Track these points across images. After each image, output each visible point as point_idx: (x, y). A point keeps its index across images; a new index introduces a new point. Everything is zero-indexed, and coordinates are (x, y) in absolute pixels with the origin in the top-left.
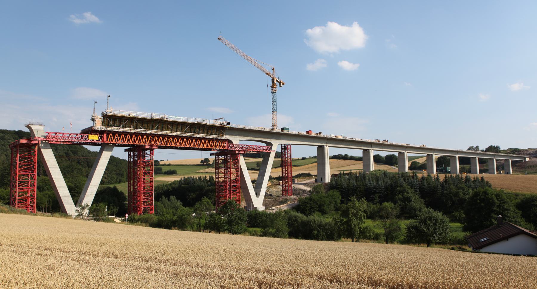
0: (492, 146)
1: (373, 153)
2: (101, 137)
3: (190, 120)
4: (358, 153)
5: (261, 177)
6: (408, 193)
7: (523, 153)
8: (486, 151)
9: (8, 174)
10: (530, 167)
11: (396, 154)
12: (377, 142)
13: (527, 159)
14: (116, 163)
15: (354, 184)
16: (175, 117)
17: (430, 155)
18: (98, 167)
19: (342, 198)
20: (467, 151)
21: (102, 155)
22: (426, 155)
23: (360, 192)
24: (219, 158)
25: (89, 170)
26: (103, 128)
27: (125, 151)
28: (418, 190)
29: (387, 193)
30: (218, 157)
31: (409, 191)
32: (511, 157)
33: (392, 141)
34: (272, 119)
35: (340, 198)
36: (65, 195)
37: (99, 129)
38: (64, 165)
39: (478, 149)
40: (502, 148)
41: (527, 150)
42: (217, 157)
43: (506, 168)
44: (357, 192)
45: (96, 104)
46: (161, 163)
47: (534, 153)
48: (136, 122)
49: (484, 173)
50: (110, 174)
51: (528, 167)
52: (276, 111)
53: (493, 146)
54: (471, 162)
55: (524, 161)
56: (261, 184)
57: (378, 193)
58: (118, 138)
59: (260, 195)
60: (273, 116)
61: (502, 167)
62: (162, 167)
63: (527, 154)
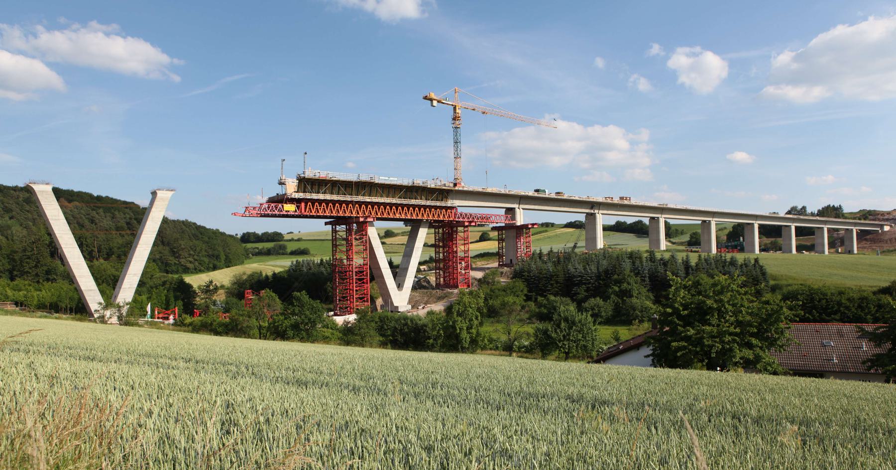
1: (602, 219)
2: (298, 207)
3: (406, 182)
5: (406, 258)
6: (629, 284)
7: (882, 217)
9: (29, 258)
10: (889, 242)
11: (646, 221)
12: (609, 201)
13: (886, 228)
14: (209, 238)
15: (549, 269)
16: (387, 178)
18: (139, 246)
19: (529, 291)
21: (146, 227)
22: (700, 222)
23: (557, 282)
24: (337, 229)
25: (164, 250)
26: (301, 195)
28: (647, 279)
29: (600, 283)
30: (336, 228)
31: (632, 281)
32: (855, 224)
35: (525, 292)
36: (90, 288)
37: (296, 197)
38: (118, 243)
39: (805, 211)
40: (846, 210)
41: (889, 213)
42: (334, 227)
43: (847, 243)
44: (552, 282)
45: (284, 162)
46: (287, 237)
48: (339, 186)
49: (806, 251)
50: (197, 255)
51: (887, 242)
54: (783, 233)
55: (880, 231)
56: (406, 269)
57: (585, 284)
58: (319, 208)
61: (838, 242)
62: (286, 243)
63: (887, 220)
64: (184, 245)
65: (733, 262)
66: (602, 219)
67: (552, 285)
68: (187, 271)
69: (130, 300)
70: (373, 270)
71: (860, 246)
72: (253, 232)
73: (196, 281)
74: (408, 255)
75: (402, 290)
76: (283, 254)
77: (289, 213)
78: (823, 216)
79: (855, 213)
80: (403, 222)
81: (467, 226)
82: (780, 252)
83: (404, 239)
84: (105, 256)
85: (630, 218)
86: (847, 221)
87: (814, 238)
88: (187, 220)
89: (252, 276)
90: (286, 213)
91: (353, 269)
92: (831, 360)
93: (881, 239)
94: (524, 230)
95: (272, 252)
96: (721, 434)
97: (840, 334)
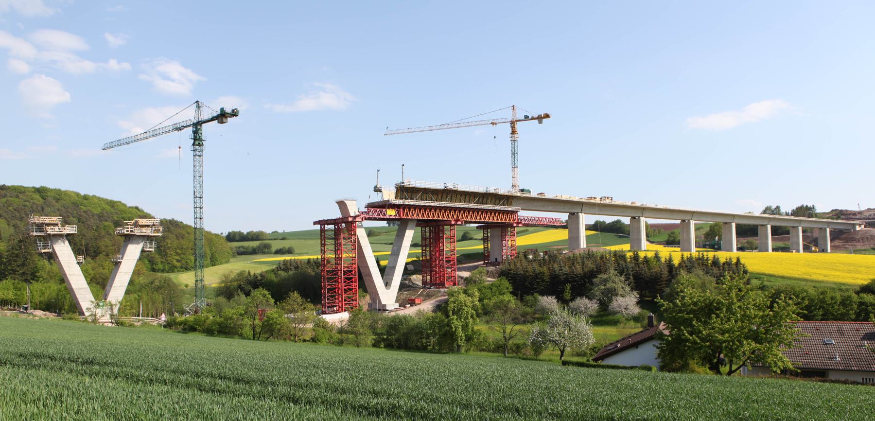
0: (803, 205)
4: (564, 217)
8: (792, 215)
10: (861, 241)
17: (686, 221)
20: (761, 216)
24: (326, 228)
26: (400, 202)
27: (314, 224)
28: (631, 277)
30: (324, 227)
33: (619, 200)
34: (513, 177)
36: (81, 287)
37: (397, 203)
39: (779, 210)
40: (819, 210)
42: (323, 227)
43: (820, 242)
47: (871, 217)
52: (517, 167)
53: (805, 206)
54: (759, 232)
59: (392, 285)
60: (513, 173)
64: (171, 244)
65: (715, 262)
66: (586, 219)
67: (538, 282)
68: (173, 269)
69: (120, 299)
70: (361, 269)
71: (833, 244)
72: (238, 231)
73: (186, 279)
74: (396, 254)
75: (389, 288)
76: (268, 253)
77: (391, 217)
78: (797, 216)
79: (828, 213)
80: (386, 222)
81: (454, 225)
82: (756, 251)
83: (392, 237)
84: (93, 254)
85: (609, 219)
86: (818, 220)
87: (789, 237)
88: (173, 219)
89: (241, 274)
90: (389, 217)
91: (341, 269)
92: (833, 358)
93: (853, 238)
94: (509, 229)
95: (257, 251)
96: (129, 417)
97: (841, 333)
